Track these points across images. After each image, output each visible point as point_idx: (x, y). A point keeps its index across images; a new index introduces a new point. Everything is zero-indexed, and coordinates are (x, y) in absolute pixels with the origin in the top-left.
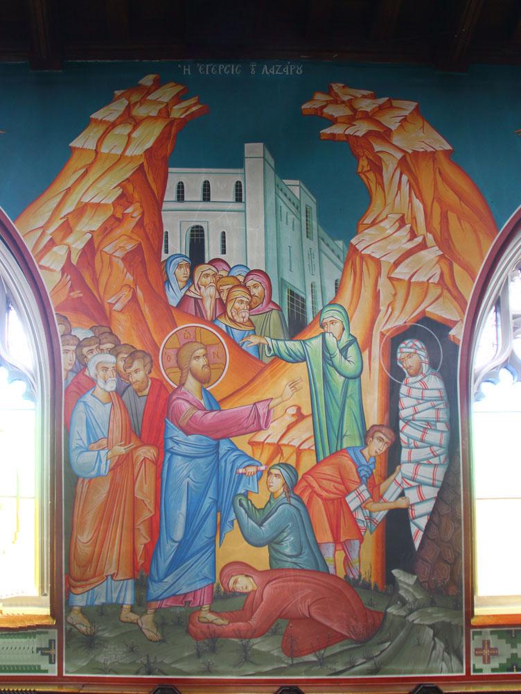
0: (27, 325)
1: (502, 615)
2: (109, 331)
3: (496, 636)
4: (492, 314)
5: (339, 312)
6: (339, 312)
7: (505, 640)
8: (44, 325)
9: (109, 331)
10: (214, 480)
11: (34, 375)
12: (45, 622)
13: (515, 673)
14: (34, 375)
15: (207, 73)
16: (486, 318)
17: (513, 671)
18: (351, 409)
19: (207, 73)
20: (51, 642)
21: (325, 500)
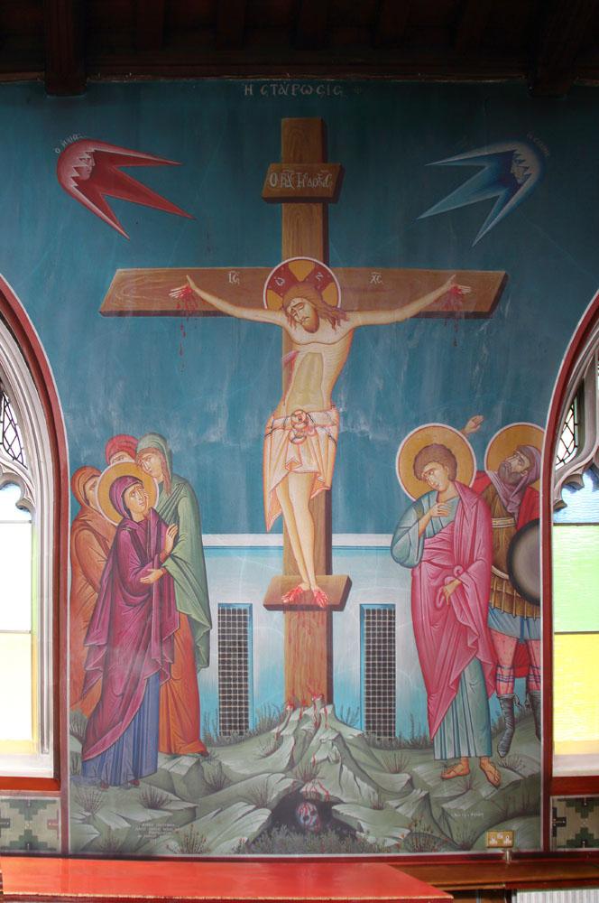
7: (574, 808)
17: (581, 847)
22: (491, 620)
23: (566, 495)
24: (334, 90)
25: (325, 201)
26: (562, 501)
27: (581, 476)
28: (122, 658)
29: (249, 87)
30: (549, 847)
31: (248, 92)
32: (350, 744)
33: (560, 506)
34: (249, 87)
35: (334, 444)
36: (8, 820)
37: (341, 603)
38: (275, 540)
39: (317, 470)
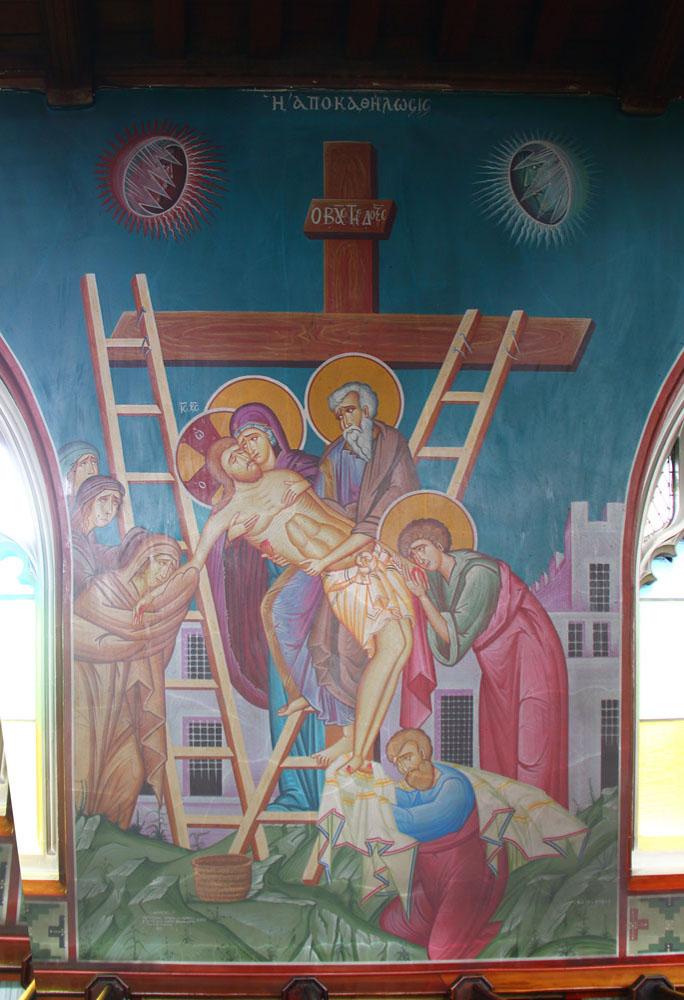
0: (14, 452)
1: (644, 876)
2: (216, 686)
3: (647, 904)
4: (668, 467)
5: (406, 643)
6: (406, 643)
7: (658, 909)
8: (35, 445)
9: (216, 686)
10: (277, 787)
11: (33, 548)
12: (51, 891)
13: (669, 953)
14: (33, 548)
15: (317, 108)
16: (657, 480)
17: (666, 950)
18: (326, 925)
19: (317, 108)
20: (61, 919)
21: (453, 612)
22: (334, 546)
23: (659, 568)
24: (395, 105)
25: (372, 239)
26: (651, 574)
27: (673, 547)
28: (527, 569)
29: (278, 100)
30: (625, 952)
31: (278, 106)
32: (433, 627)
33: (649, 580)
34: (278, 100)
35: (520, 760)
36: (50, 935)
37: (574, 363)
38: (211, 683)
39: (471, 650)
